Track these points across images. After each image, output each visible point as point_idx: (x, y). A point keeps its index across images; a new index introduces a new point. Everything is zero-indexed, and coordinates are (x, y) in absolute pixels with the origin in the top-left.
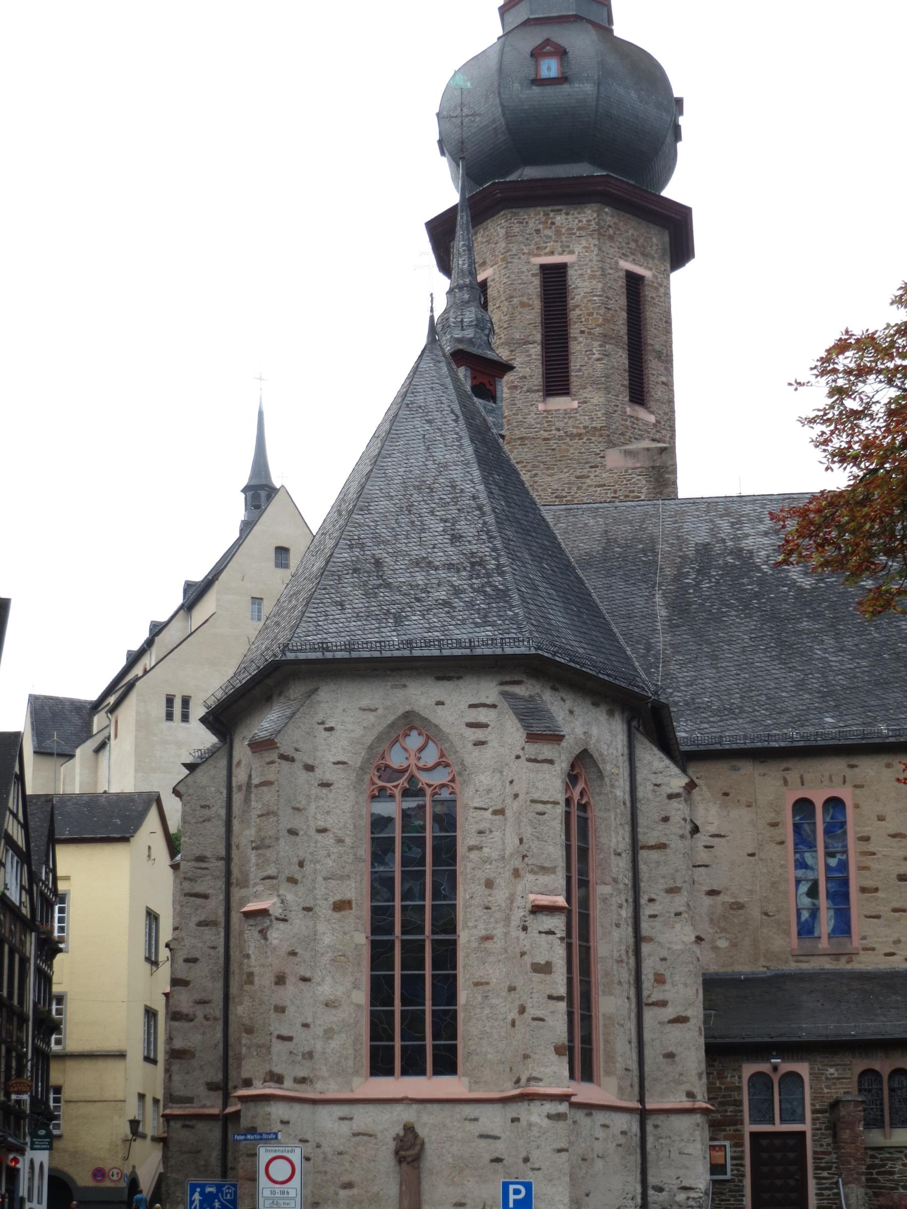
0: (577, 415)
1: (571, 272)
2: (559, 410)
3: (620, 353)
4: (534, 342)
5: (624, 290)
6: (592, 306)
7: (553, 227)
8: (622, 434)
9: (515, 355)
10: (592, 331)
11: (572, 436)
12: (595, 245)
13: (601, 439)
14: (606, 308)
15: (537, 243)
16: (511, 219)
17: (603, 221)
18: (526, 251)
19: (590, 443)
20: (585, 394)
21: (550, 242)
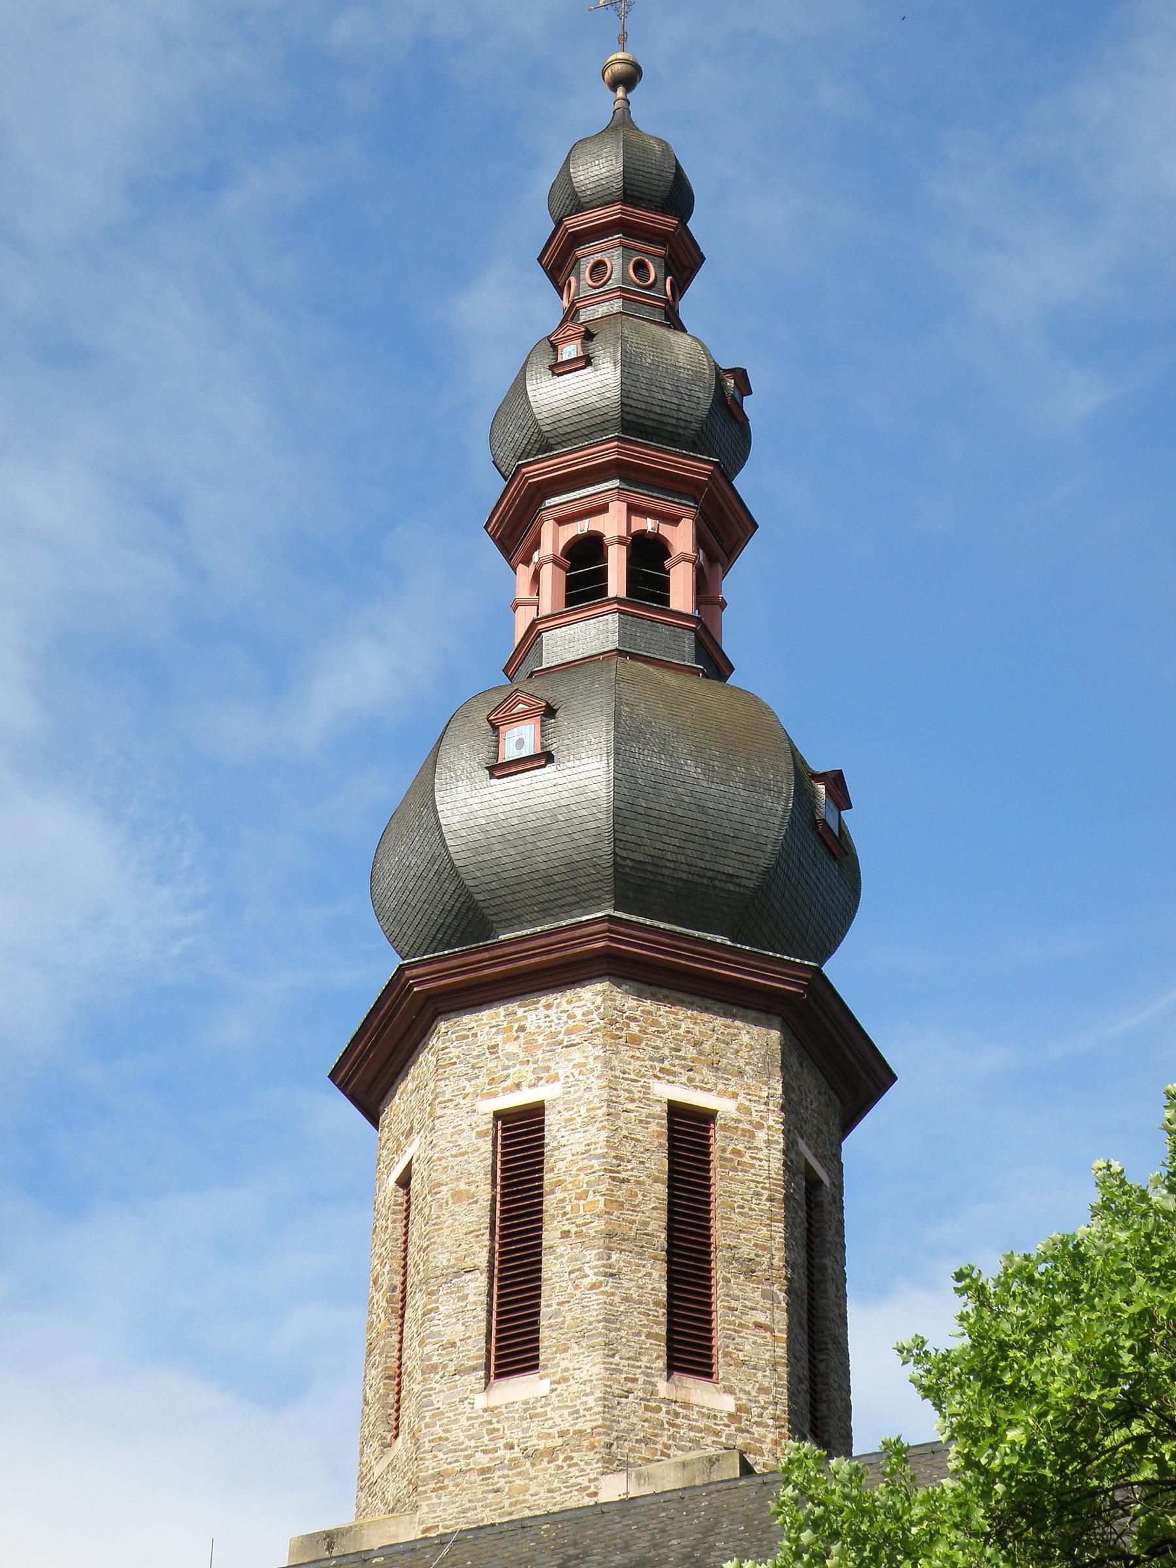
0: (548, 1409)
1: (550, 1118)
5: (664, 1141)
6: (587, 1178)
7: (522, 1035)
8: (645, 1441)
10: (584, 1229)
11: (533, 1456)
13: (591, 1454)
14: (613, 1179)
15: (491, 1072)
18: (469, 1090)
19: (570, 1466)
20: (564, 1362)
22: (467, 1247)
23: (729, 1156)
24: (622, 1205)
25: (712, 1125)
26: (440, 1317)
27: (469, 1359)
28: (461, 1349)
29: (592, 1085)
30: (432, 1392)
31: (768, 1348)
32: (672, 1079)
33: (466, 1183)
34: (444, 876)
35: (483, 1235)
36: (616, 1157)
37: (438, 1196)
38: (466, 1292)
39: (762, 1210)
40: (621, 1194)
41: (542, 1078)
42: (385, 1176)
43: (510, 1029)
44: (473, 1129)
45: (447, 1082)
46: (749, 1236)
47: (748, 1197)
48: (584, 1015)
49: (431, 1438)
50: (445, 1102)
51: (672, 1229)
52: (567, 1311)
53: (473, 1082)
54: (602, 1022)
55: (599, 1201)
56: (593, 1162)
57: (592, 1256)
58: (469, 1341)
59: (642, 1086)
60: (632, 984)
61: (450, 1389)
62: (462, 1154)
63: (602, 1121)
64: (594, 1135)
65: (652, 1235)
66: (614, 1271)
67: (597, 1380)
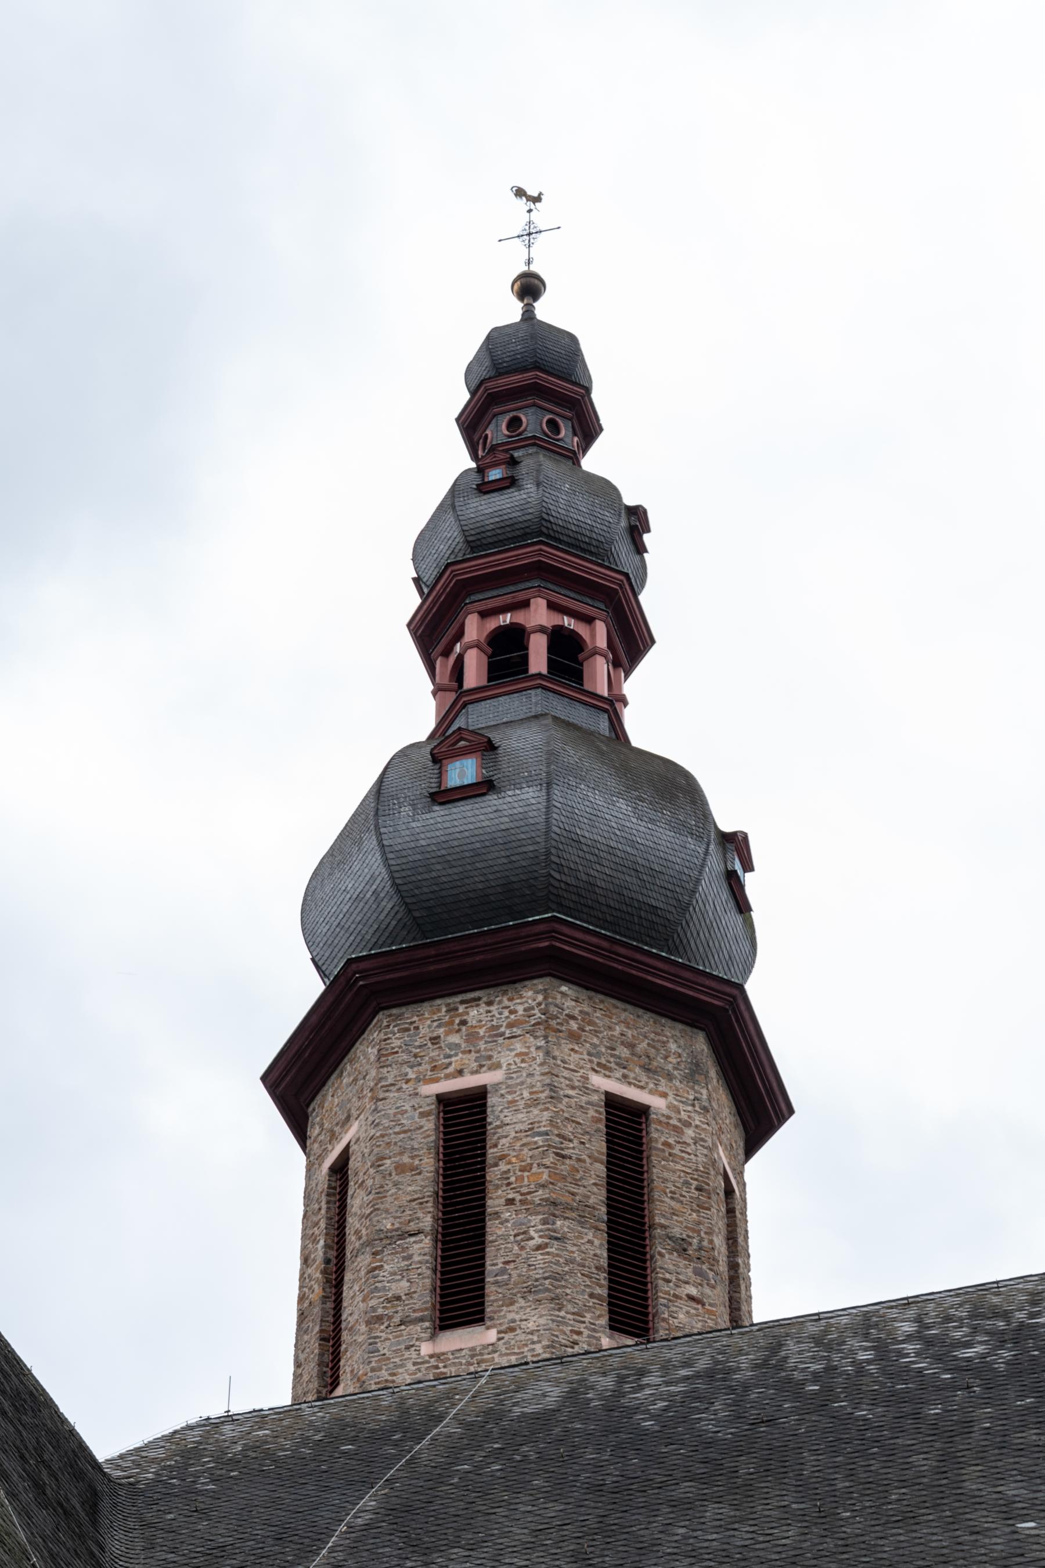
0: (496, 1355)
1: (492, 1100)
2: (461, 1350)
3: (590, 1236)
4: (419, 1232)
6: (531, 1153)
7: (464, 1028)
9: (381, 1260)
10: (529, 1197)
12: (538, 1048)
14: (557, 1154)
15: (433, 1060)
16: (388, 1026)
17: (556, 1006)
20: (511, 1315)
21: (456, 1055)
22: (411, 1212)
23: (661, 1147)
24: (564, 1178)
25: (643, 1120)
26: (385, 1274)
27: (414, 1311)
28: (406, 1302)
29: (534, 1072)
30: (378, 1340)
31: (700, 1318)
32: (607, 1073)
33: (409, 1157)
34: (382, 895)
35: (427, 1202)
36: (558, 1135)
37: (382, 1168)
38: (410, 1252)
39: (691, 1197)
40: (564, 1168)
41: (484, 1066)
42: (317, 1166)
43: (452, 1023)
44: (415, 1110)
45: (389, 1069)
46: (681, 1219)
47: (679, 1185)
48: (525, 1010)
49: (377, 1380)
50: (387, 1086)
51: (611, 1203)
52: (512, 1269)
53: (415, 1069)
54: (543, 1016)
55: (543, 1172)
56: (536, 1139)
57: (538, 1221)
58: (414, 1295)
59: (581, 1077)
60: (571, 986)
61: (396, 1337)
62: (405, 1132)
63: (545, 1103)
64: (537, 1115)
65: (594, 1208)
66: (559, 1236)
67: (545, 1330)
